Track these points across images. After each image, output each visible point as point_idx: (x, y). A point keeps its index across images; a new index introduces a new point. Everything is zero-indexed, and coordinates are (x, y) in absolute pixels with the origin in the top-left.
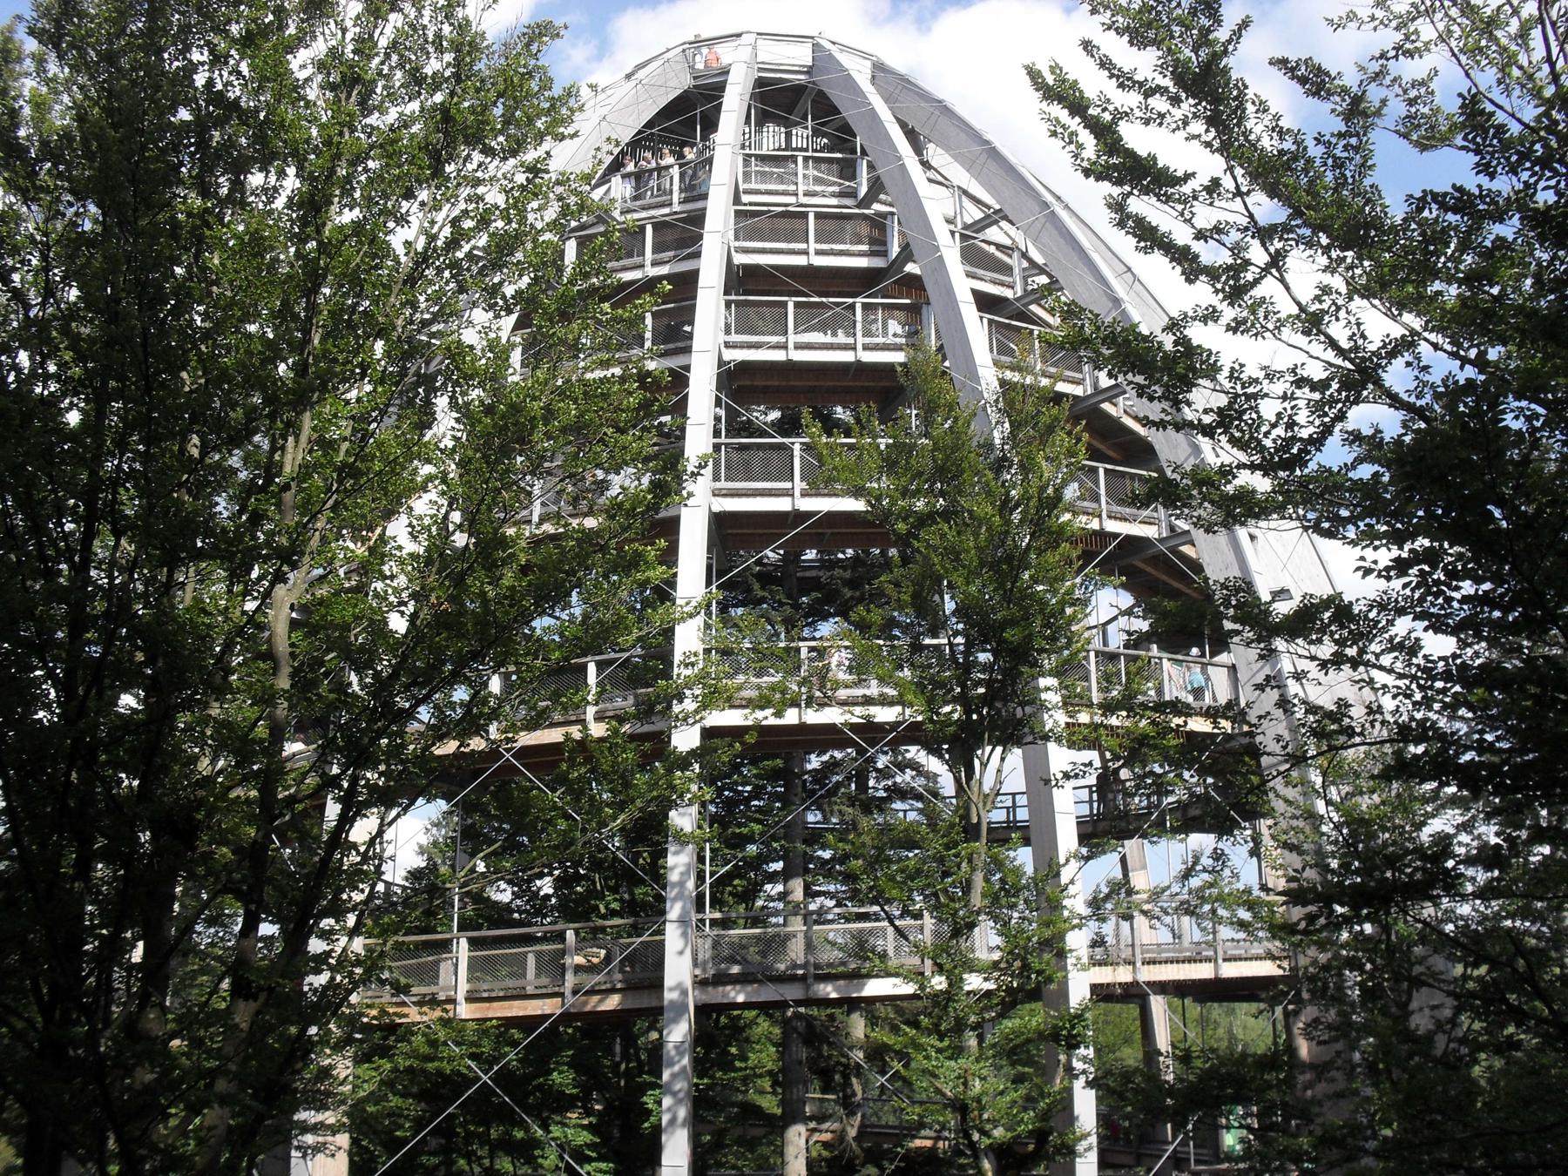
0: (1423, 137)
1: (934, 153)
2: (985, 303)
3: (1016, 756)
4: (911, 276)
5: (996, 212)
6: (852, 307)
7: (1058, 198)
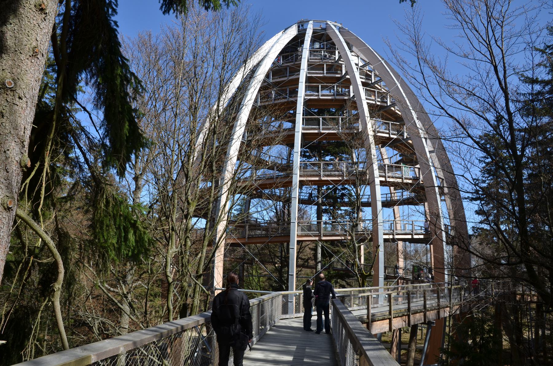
0: (197, 206)
1: (354, 49)
2: (364, 84)
3: (368, 188)
4: (348, 78)
5: (368, 63)
6: (334, 86)
7: (383, 59)
